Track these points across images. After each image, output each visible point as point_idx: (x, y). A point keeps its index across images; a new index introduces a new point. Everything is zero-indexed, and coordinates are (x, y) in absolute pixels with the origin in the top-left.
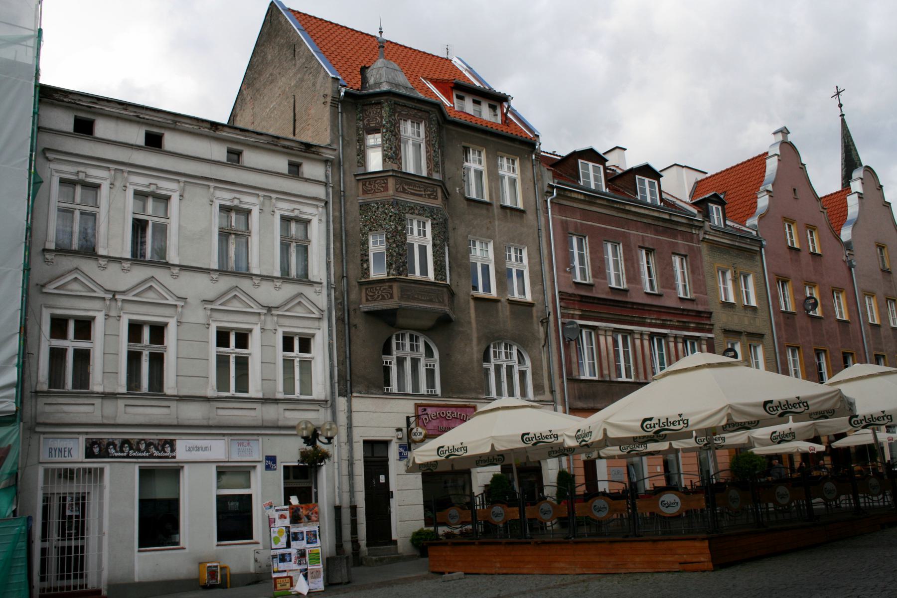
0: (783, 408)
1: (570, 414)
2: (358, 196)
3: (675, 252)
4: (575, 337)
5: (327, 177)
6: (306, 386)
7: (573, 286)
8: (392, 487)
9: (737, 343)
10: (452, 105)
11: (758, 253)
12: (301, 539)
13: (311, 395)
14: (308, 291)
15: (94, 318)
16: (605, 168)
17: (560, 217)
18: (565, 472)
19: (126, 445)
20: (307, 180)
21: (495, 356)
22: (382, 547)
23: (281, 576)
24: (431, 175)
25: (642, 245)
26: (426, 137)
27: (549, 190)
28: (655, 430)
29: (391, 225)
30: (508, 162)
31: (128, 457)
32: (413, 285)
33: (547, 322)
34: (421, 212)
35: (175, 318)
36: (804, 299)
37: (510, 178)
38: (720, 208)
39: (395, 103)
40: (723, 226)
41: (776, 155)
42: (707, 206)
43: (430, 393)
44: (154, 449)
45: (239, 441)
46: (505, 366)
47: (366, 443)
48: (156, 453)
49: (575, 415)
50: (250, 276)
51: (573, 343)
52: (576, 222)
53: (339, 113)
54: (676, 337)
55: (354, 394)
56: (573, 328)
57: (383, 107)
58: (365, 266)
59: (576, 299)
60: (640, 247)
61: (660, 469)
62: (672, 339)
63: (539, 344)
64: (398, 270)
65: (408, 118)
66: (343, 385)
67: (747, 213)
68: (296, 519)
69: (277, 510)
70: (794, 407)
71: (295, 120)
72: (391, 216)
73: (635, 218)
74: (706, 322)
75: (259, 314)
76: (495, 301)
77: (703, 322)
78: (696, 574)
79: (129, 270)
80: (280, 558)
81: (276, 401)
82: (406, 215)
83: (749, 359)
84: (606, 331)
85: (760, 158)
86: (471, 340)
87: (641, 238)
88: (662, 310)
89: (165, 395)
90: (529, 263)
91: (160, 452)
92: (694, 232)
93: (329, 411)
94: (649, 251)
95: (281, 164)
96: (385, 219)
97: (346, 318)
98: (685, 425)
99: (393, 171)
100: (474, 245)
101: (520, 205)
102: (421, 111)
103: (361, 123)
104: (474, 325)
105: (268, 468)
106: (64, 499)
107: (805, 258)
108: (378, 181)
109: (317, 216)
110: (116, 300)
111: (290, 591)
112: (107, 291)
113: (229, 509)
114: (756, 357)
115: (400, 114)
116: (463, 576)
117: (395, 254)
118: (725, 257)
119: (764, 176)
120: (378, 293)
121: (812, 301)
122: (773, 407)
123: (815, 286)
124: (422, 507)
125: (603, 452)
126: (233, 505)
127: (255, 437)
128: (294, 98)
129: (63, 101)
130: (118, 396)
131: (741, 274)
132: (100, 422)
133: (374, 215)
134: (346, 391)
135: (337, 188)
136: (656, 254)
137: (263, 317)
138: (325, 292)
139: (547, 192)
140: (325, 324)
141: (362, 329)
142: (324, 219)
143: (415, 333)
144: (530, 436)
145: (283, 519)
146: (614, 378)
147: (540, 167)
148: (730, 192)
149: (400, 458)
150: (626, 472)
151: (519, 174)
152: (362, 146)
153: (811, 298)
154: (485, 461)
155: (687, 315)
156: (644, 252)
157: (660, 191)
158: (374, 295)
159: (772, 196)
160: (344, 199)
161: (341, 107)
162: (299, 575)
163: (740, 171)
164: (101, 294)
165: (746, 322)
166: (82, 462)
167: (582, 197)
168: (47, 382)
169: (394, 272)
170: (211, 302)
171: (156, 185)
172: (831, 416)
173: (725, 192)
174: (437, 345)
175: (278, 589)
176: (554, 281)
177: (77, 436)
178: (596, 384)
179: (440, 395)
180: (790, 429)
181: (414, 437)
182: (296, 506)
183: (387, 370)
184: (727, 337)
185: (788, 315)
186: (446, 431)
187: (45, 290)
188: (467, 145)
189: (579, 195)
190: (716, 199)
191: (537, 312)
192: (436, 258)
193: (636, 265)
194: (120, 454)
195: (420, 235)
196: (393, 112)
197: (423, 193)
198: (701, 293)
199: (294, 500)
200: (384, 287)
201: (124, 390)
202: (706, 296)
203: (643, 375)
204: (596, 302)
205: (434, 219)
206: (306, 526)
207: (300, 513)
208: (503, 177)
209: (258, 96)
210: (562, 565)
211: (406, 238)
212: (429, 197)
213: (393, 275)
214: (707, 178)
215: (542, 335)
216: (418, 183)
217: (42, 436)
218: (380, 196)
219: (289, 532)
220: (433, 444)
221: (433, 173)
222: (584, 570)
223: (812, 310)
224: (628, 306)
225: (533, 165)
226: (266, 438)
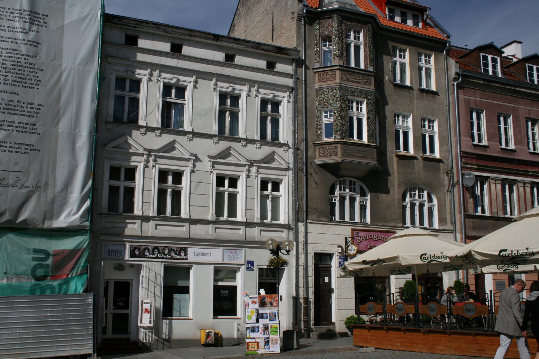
2: (315, 84)
8: (333, 286)
16: (502, 58)
17: (464, 96)
18: (460, 282)
19: (156, 250)
23: (252, 341)
24: (367, 67)
29: (337, 104)
31: (157, 258)
34: (359, 95)
43: (362, 222)
44: (173, 253)
46: (417, 204)
47: (315, 254)
48: (175, 256)
52: (477, 100)
56: (470, 178)
57: (333, 20)
58: (319, 132)
63: (444, 189)
68: (263, 304)
69: (250, 298)
71: (273, 30)
72: (337, 98)
80: (251, 330)
84: (496, 181)
90: (439, 130)
91: (178, 256)
105: (248, 269)
111: (257, 351)
113: (222, 295)
117: (340, 124)
120: (327, 151)
126: (225, 292)
128: (273, 15)
133: (326, 97)
138: (291, 151)
168: (107, 208)
169: (339, 137)
171: (178, 78)
172: (523, 263)
175: (249, 349)
179: (369, 223)
181: (349, 252)
182: (264, 296)
183: (333, 205)
186: (371, 249)
192: (369, 127)
194: (152, 256)
197: (361, 81)
199: (263, 292)
200: (331, 147)
205: (369, 99)
207: (266, 301)
209: (249, 12)
212: (365, 84)
218: (330, 84)
219: (258, 312)
220: (360, 258)
221: (368, 66)
222: (457, 352)
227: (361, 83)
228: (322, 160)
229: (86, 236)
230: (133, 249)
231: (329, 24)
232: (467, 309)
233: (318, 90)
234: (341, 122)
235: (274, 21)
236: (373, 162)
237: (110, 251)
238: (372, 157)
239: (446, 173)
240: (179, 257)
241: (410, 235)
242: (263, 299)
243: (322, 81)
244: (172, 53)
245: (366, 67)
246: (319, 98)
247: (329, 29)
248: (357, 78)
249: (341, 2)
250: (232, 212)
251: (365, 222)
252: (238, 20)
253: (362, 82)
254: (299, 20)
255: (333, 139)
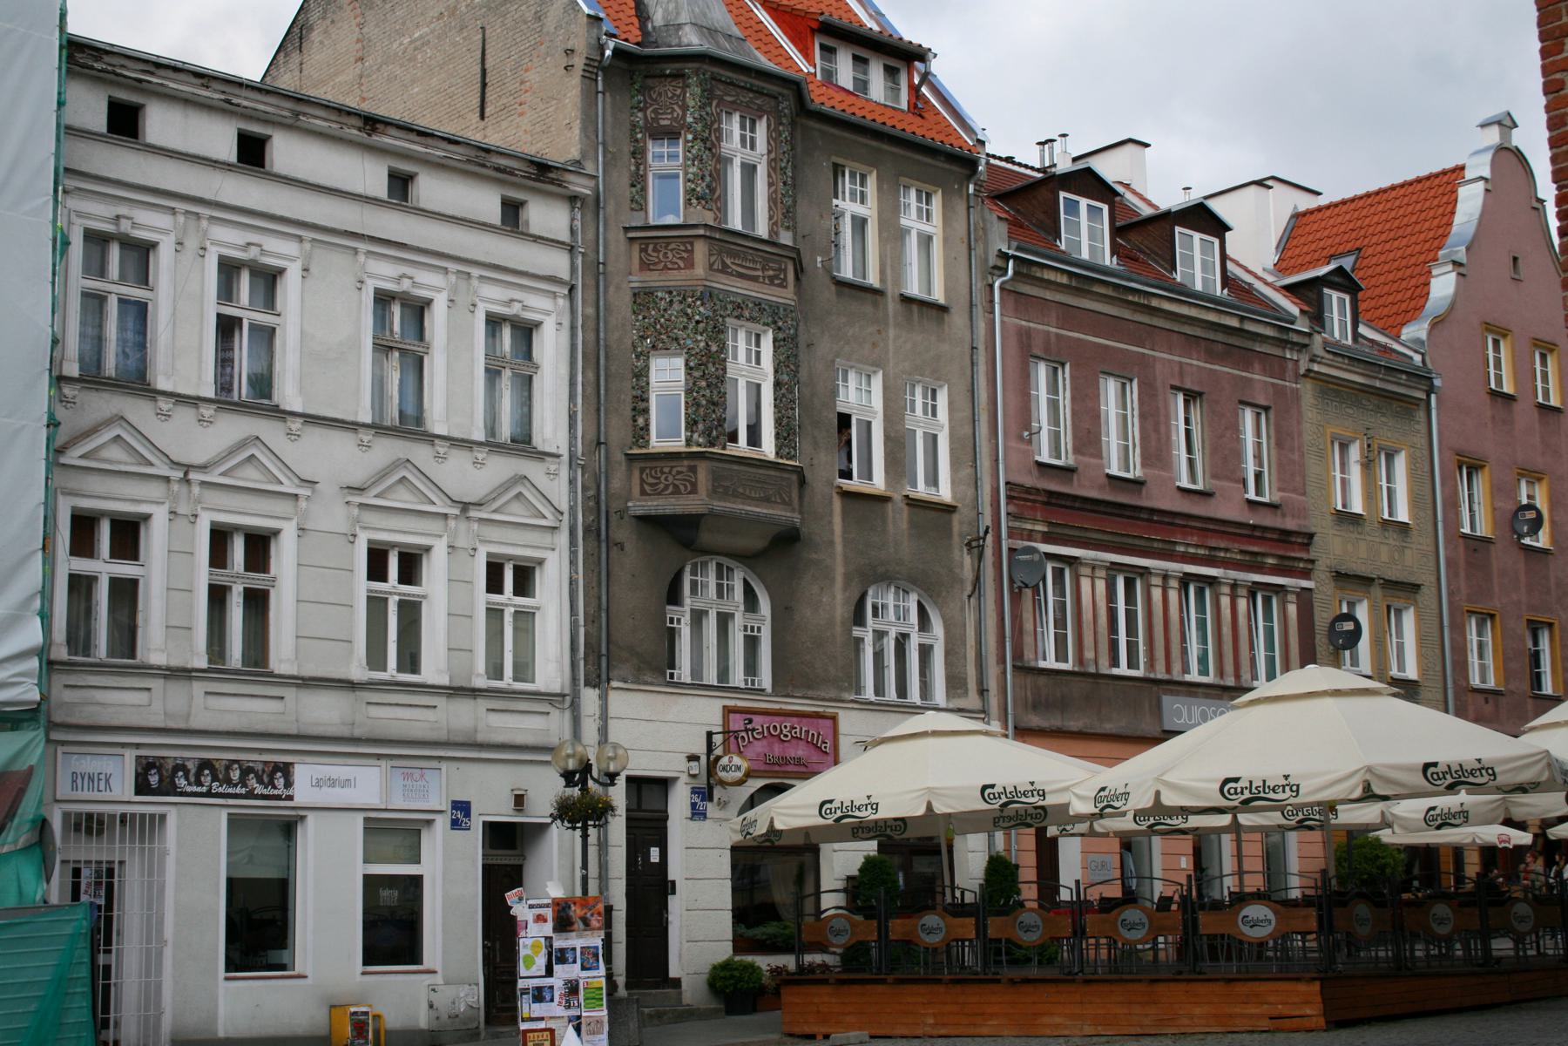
0: (1454, 775)
1: (1014, 739)
2: (630, 274)
3: (1245, 399)
4: (1033, 584)
5: (572, 232)
6: (524, 669)
7: (1035, 471)
8: (673, 873)
9: (1360, 601)
10: (812, 70)
11: (1423, 405)
12: (571, 960)
13: (533, 682)
14: (533, 470)
15: (147, 517)
17: (1017, 321)
18: (1001, 857)
19: (207, 772)
20: (537, 239)
21: (875, 614)
22: (653, 991)
24: (777, 234)
25: (1178, 384)
26: (769, 152)
27: (1000, 263)
28: (1243, 797)
29: (697, 341)
30: (919, 200)
31: (209, 794)
32: (735, 467)
33: (981, 549)
34: (755, 314)
35: (294, 523)
36: (1514, 508)
37: (920, 235)
38: (1347, 298)
39: (713, 78)
40: (1350, 342)
41: (1482, 178)
42: (1321, 296)
43: (750, 686)
44: (254, 780)
45: (406, 771)
48: (259, 790)
49: (1024, 742)
50: (430, 438)
51: (1028, 592)
52: (1048, 333)
53: (598, 92)
54: (1234, 586)
55: (614, 684)
58: (641, 421)
59: (1039, 498)
60: (1173, 387)
61: (1185, 863)
62: (1226, 590)
63: (962, 590)
64: (709, 435)
65: (735, 110)
66: (593, 665)
67: (1404, 306)
69: (531, 907)
70: (1473, 775)
71: (484, 85)
73: (1168, 325)
74: (1298, 555)
75: (446, 516)
76: (883, 499)
77: (1293, 555)
78: (1298, 1034)
79: (211, 422)
80: (534, 996)
81: (474, 693)
82: (727, 319)
83: (1385, 638)
84: (1094, 568)
85: (1445, 179)
86: (833, 580)
87: (1177, 369)
88: (1211, 527)
89: (271, 675)
90: (951, 420)
91: (266, 787)
92: (1288, 356)
93: (567, 714)
94: (1191, 397)
95: (485, 202)
96: (685, 328)
97: (603, 528)
98: (1294, 794)
99: (706, 225)
100: (845, 380)
101: (938, 295)
102: (762, 94)
103: (640, 114)
104: (839, 548)
105: (455, 824)
106: (77, 873)
107: (1524, 414)
108: (672, 246)
109: (554, 315)
110: (188, 482)
112: (175, 464)
114: (1400, 634)
115: (721, 101)
116: (867, 1039)
117: (704, 402)
118: (1351, 412)
119: (1450, 224)
120: (666, 479)
121: (1531, 515)
122: (1437, 774)
123: (1540, 480)
124: (728, 916)
125: (1101, 825)
126: (388, 896)
127: (434, 764)
129: (92, 68)
130: (194, 674)
131: (1381, 449)
132: (161, 725)
133: (663, 316)
134: (599, 676)
135: (592, 256)
136: (1204, 404)
137: (452, 523)
138: (564, 473)
139: (995, 267)
140: (563, 538)
141: (632, 556)
142: (566, 323)
143: (726, 561)
144: (995, 790)
145: (541, 924)
146: (1105, 669)
147: (982, 210)
148: (1370, 251)
149: (693, 814)
150: (1118, 865)
151: (940, 224)
152: (642, 167)
153: (1530, 507)
154: (870, 830)
155: (1260, 538)
156: (1180, 398)
157: (1224, 257)
158: (656, 484)
159: (1463, 275)
160: (605, 280)
161: (604, 80)
162: (567, 1027)
163: (1397, 203)
164: (164, 470)
165: (1384, 557)
166: (129, 802)
167: (1064, 280)
169: (701, 440)
170: (360, 490)
171: (260, 246)
173: (1359, 249)
174: (768, 588)
176: (997, 460)
177: (119, 750)
178: (1069, 678)
180: (1462, 804)
181: (722, 775)
183: (672, 635)
184: (1341, 589)
185: (1476, 544)
187: (63, 460)
188: (840, 161)
189: (1059, 275)
190: (1342, 280)
191: (961, 523)
192: (779, 412)
193: (1162, 428)
194: (195, 789)
195: (751, 362)
196: (708, 96)
197: (760, 273)
198: (1294, 491)
200: (679, 469)
201: (204, 664)
202: (1304, 498)
203: (1164, 663)
204: (1077, 505)
205: (779, 329)
206: (580, 937)
207: (572, 914)
208: (908, 231)
210: (1058, 1020)
211: (724, 370)
212: (772, 283)
213: (699, 445)
214: (1319, 209)
215: (968, 573)
216: (751, 251)
217: (60, 749)
218: (676, 278)
219: (551, 946)
222: (1100, 1028)
223: (1528, 534)
224: (1142, 516)
225: (969, 208)
226: (454, 765)
227: (761, 280)
228: (650, 503)
229: (35, 733)
230: (143, 769)
231: (674, 95)
232: (1127, 922)
233: (639, 293)
234: (708, 395)
235: (488, 56)
236: (789, 514)
237: (79, 777)
238: (787, 499)
239: (966, 545)
240: (270, 791)
241: (935, 734)
242: (564, 909)
243: (652, 267)
244: (240, 165)
245: (772, 232)
246: (640, 317)
247: (674, 110)
248: (751, 265)
249: (702, 27)
250: (410, 660)
251: (756, 687)
252: (325, 11)
253: (764, 277)
254: (587, 75)
255: (683, 443)
